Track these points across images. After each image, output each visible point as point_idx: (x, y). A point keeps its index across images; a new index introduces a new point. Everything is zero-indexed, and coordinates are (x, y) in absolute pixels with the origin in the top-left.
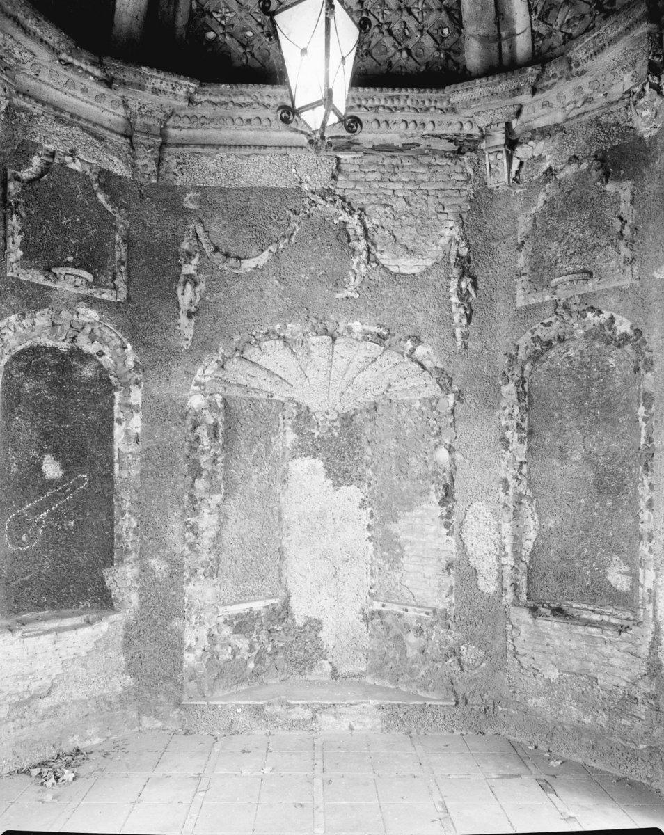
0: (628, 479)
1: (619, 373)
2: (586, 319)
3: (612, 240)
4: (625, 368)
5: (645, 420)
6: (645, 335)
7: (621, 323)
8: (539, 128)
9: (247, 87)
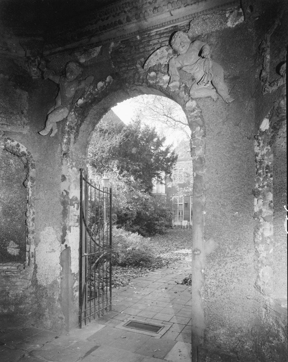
0: (18, 209)
1: (14, 166)
2: (7, 142)
4: (17, 165)
5: (31, 187)
7: (22, 147)
8: (195, 169)
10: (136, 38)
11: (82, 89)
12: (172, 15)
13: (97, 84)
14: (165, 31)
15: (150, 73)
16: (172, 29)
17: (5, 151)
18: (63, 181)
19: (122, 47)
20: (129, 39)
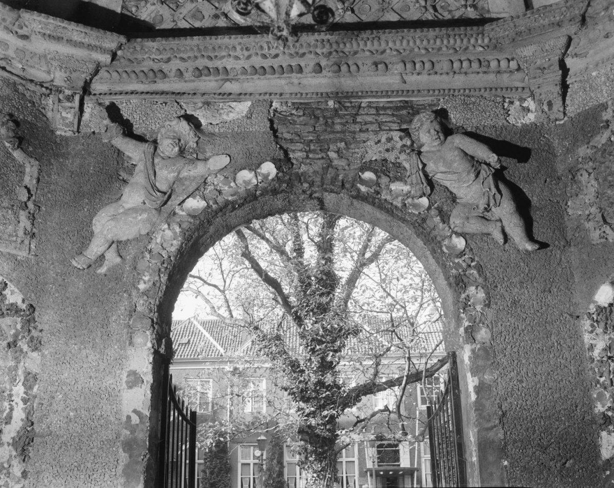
3: (13, 206)
6: (36, 313)
7: (12, 293)
9: (186, 39)
10: (327, 105)
11: (195, 178)
12: (405, 82)
13: (235, 173)
14: (388, 105)
15: (363, 173)
16: (402, 105)
17: (542, 67)
18: (130, 387)
19: (296, 113)
20: (310, 103)
